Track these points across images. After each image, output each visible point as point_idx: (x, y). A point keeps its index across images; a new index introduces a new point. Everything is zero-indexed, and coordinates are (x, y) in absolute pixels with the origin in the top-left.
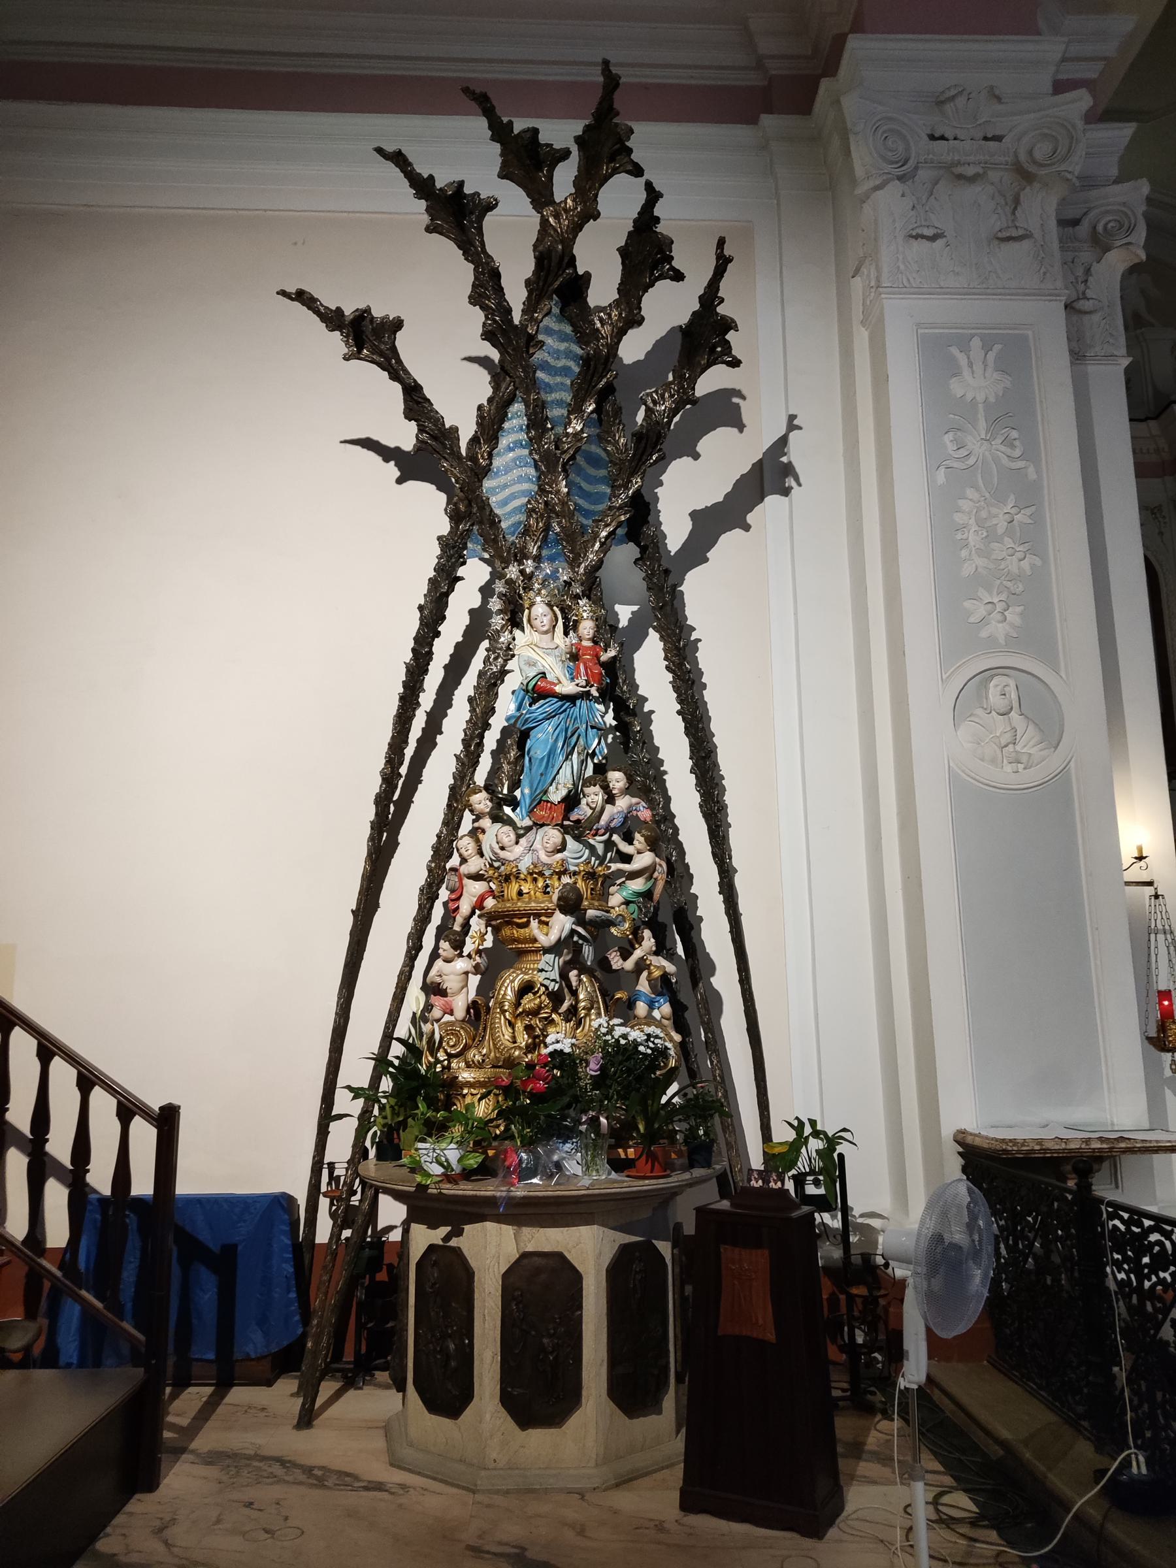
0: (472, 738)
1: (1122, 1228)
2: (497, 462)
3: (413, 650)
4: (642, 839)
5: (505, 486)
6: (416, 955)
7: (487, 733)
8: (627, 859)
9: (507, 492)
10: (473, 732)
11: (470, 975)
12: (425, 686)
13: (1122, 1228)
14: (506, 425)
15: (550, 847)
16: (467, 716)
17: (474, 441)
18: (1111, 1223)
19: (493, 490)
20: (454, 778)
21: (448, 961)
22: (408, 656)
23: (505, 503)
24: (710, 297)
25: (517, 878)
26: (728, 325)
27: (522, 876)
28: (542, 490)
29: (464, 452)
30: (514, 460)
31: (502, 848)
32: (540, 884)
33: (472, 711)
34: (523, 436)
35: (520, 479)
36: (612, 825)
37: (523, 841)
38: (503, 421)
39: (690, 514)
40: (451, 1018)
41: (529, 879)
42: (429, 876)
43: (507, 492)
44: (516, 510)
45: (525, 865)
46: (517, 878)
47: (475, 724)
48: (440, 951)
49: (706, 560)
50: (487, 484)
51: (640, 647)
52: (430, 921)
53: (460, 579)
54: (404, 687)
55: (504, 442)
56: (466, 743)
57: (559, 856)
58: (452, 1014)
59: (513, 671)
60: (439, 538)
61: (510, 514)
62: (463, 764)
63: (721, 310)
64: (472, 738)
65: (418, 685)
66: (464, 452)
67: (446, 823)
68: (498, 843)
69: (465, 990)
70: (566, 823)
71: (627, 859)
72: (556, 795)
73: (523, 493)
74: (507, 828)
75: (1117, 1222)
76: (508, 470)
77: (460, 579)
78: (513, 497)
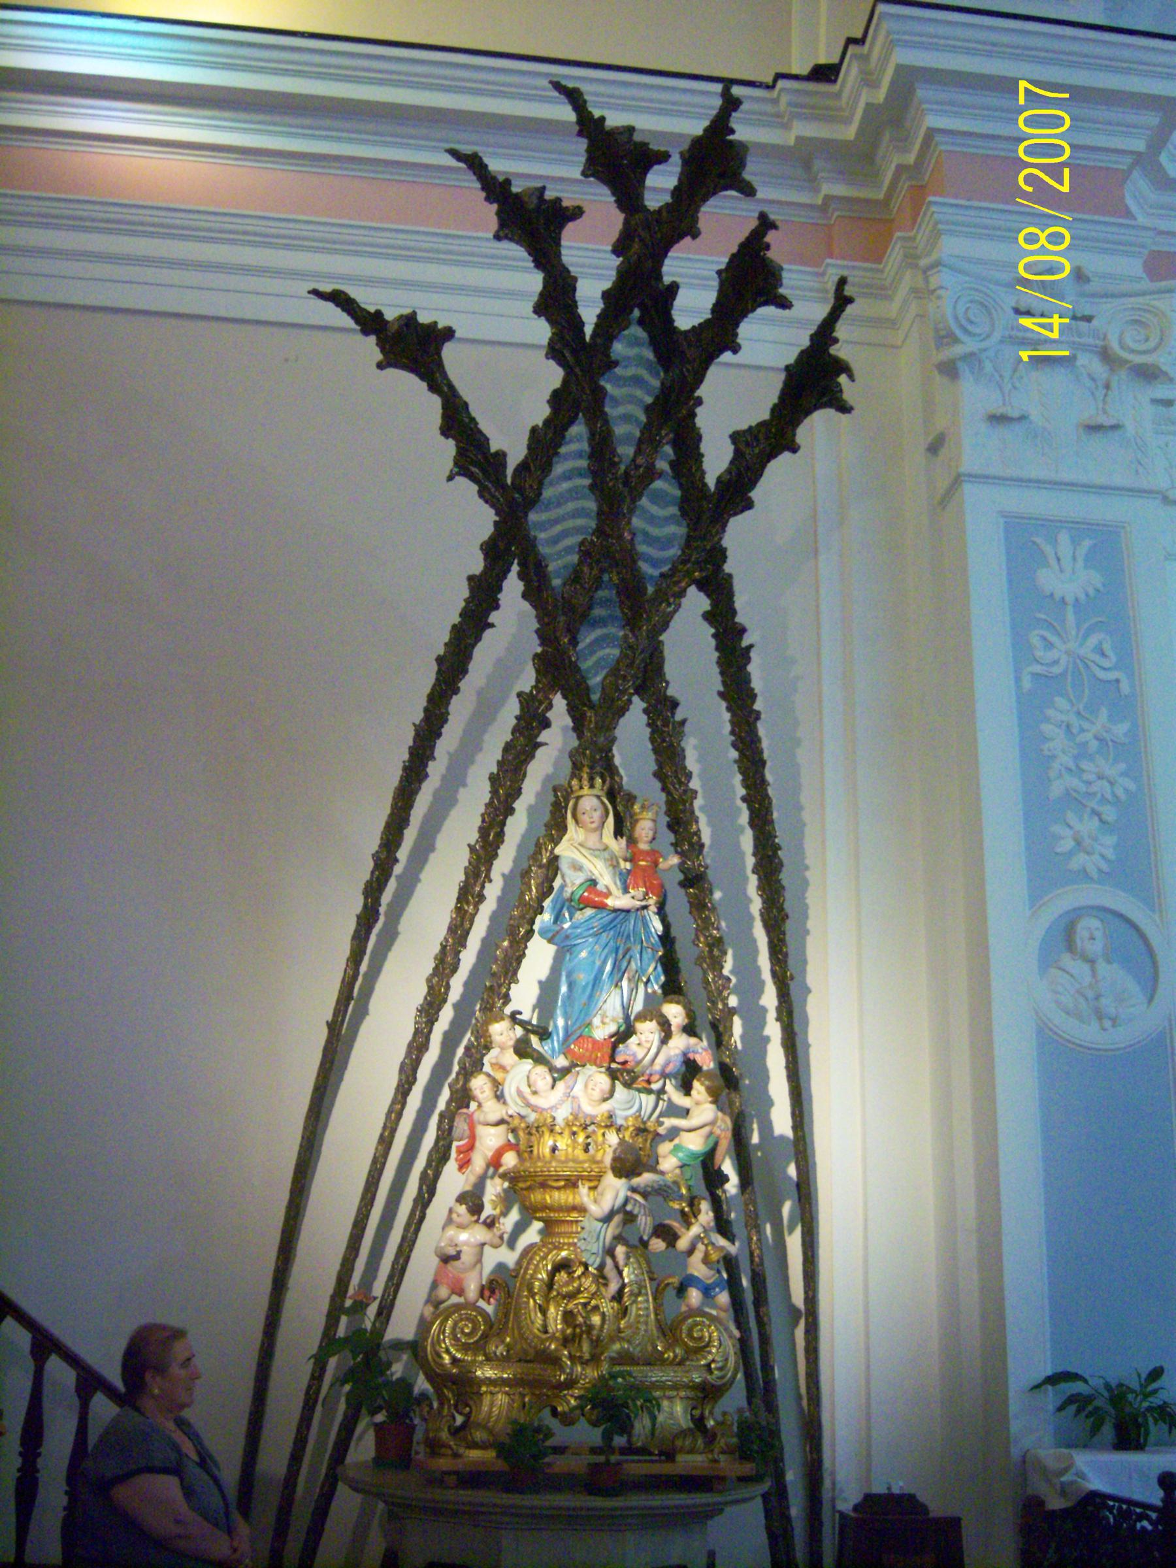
0: (491, 826)
1: (1150, 1528)
2: (548, 493)
3: (426, 710)
4: (702, 1089)
5: (556, 522)
6: (410, 1089)
7: (510, 820)
8: (686, 1113)
9: (559, 528)
10: (494, 819)
11: (487, 1248)
12: (436, 754)
13: (1150, 1528)
14: (563, 450)
15: (597, 1095)
16: (487, 797)
17: (523, 467)
18: (1138, 1525)
19: (542, 526)
20: (466, 874)
21: (462, 1227)
22: (418, 716)
23: (555, 541)
24: (824, 334)
25: (552, 1131)
26: (842, 367)
27: (557, 1129)
28: (600, 531)
29: (509, 481)
30: (570, 490)
31: (535, 1093)
32: (581, 1138)
33: (494, 792)
34: (583, 463)
35: (576, 514)
36: (668, 1070)
37: (561, 1085)
38: (560, 445)
39: (731, 436)
40: (462, 1300)
41: (567, 1133)
42: (429, 993)
43: (559, 528)
44: (568, 550)
45: (562, 1115)
46: (552, 1131)
47: (496, 809)
48: (454, 1216)
49: (749, 505)
50: (533, 517)
51: (768, 1077)
52: (427, 1049)
53: (492, 626)
54: (411, 754)
55: (559, 469)
56: (484, 832)
57: (606, 1106)
58: (460, 1295)
59: (546, 744)
60: (471, 578)
61: (559, 555)
62: (479, 857)
63: (833, 350)
64: (491, 826)
65: (428, 753)
66: (509, 481)
67: (452, 930)
68: (529, 1086)
69: (478, 1266)
70: (614, 1065)
71: (686, 1113)
72: (602, 1030)
73: (577, 530)
74: (541, 1070)
75: (1145, 1523)
76: (559, 502)
77: (492, 626)
78: (565, 534)
